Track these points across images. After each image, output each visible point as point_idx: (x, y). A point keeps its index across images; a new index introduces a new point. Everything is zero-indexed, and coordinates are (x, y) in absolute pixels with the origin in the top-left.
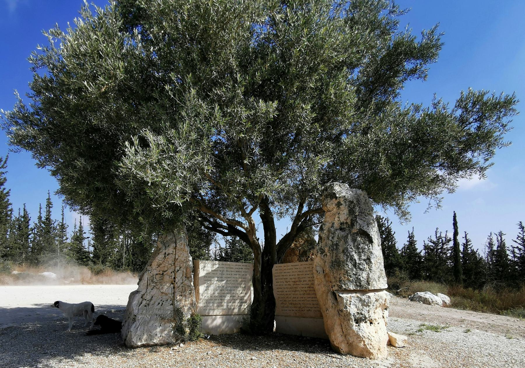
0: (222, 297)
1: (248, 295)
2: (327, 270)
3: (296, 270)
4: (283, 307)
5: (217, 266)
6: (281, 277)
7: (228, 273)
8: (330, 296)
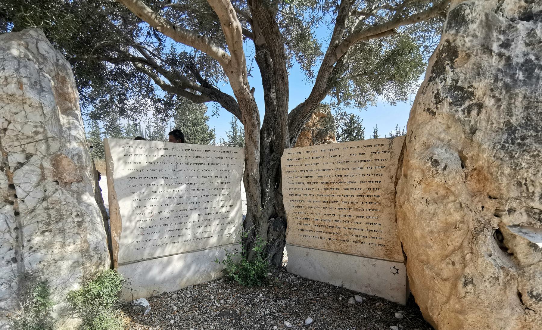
0: (180, 218)
1: (236, 209)
2: (485, 155)
3: (332, 160)
5: (162, 153)
6: (300, 174)
7: (191, 167)
8: (487, 243)
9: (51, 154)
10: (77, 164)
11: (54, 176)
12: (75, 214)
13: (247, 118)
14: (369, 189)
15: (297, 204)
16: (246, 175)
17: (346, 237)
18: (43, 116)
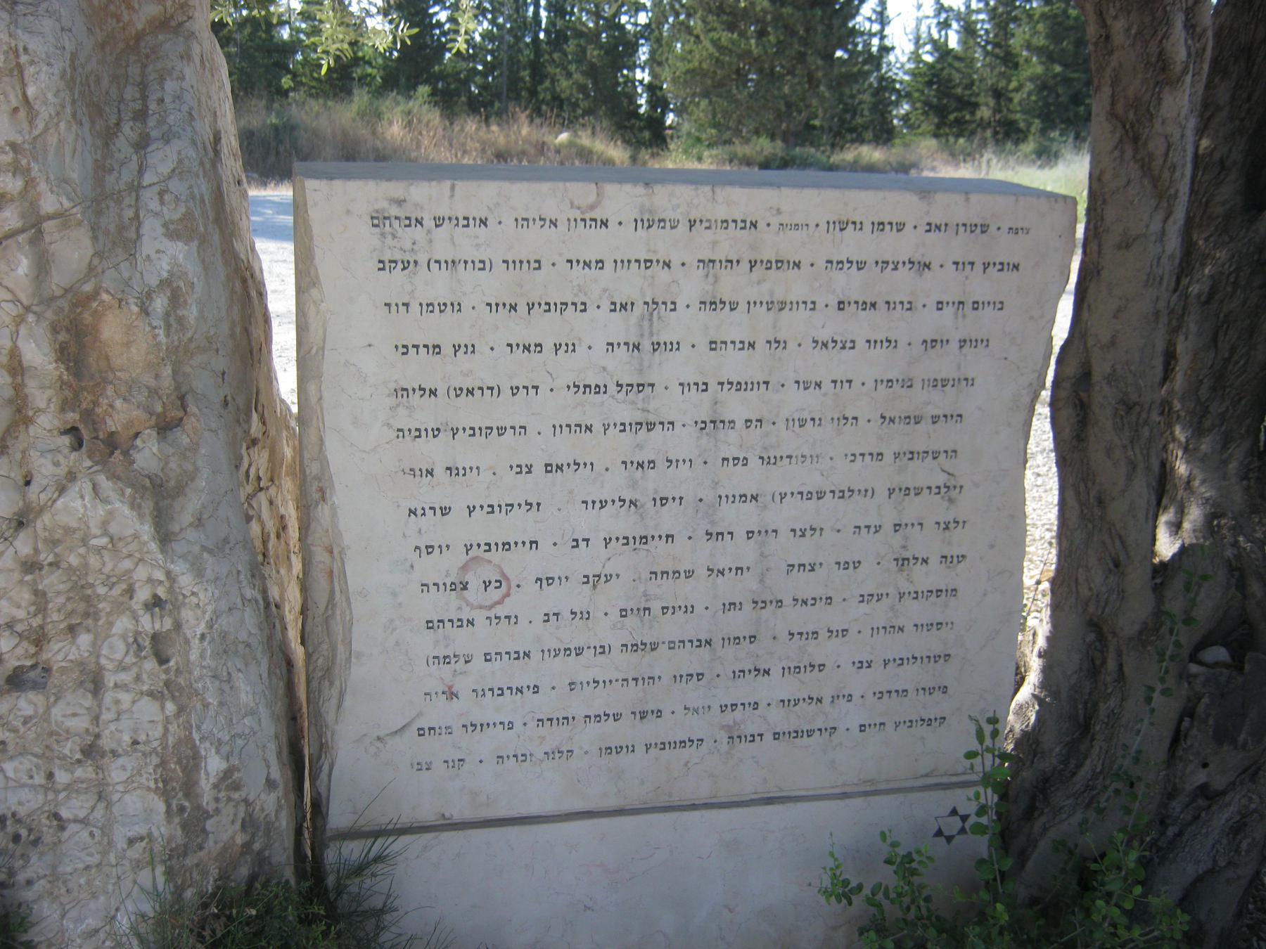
7: (735, 326)
9: (53, 299)
10: (162, 338)
11: (64, 407)
12: (143, 594)
13: (1118, 26)
16: (1072, 369)
18: (22, 114)
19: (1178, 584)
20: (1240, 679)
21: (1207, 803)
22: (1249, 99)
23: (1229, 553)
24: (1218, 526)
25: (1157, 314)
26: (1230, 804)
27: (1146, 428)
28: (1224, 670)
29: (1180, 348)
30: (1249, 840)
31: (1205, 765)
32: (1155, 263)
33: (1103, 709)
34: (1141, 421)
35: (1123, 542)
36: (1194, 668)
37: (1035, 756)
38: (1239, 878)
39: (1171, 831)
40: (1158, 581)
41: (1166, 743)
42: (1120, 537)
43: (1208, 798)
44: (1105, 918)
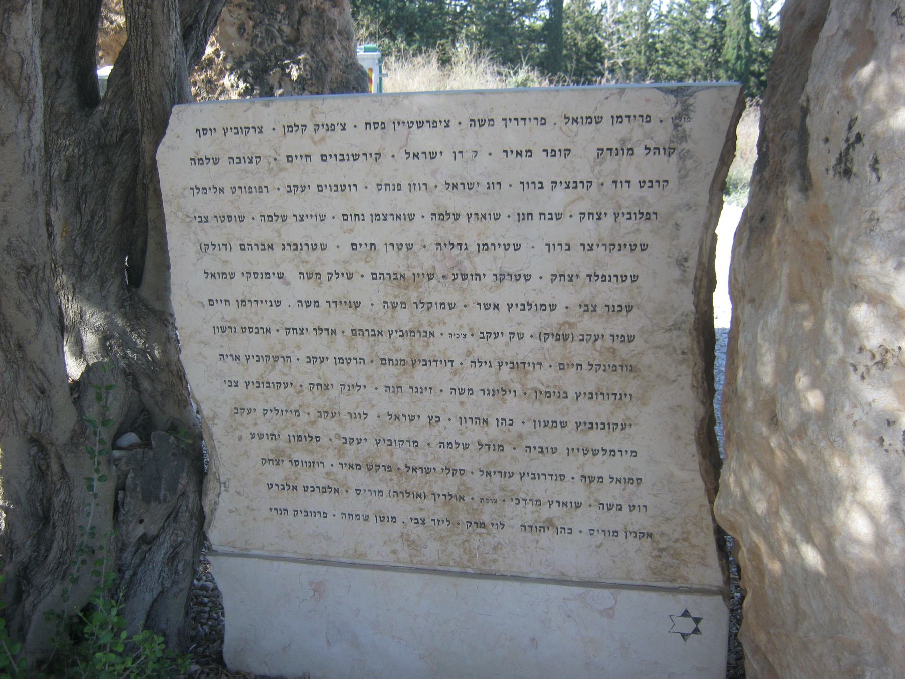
4: (288, 487)
14: (589, 308)
15: (256, 370)
17: (489, 508)
19: (91, 395)
20: (151, 453)
21: (148, 547)
22: (69, 24)
23: (122, 363)
24: (110, 345)
25: (35, 194)
26: (163, 543)
27: (44, 283)
28: (139, 450)
29: (54, 217)
30: (183, 563)
31: (141, 521)
32: (27, 155)
33: (57, 502)
34: (39, 278)
35: (44, 374)
36: (117, 453)
37: (12, 552)
38: (181, 590)
39: (127, 575)
40: (76, 396)
41: (111, 514)
42: (41, 370)
43: (149, 543)
44: (104, 665)
